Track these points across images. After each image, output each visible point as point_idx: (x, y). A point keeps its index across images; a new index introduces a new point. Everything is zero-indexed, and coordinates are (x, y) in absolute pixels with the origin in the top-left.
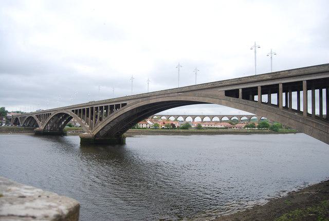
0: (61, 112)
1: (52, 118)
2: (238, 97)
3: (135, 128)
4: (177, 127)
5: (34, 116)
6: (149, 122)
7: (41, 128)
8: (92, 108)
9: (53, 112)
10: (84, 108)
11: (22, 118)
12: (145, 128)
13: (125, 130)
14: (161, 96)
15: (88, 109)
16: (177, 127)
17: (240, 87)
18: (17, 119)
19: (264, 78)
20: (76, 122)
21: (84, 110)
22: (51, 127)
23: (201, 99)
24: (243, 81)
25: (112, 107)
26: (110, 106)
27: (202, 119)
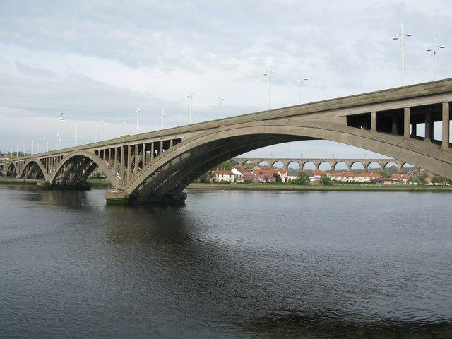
0: (77, 154)
1: (66, 163)
2: (369, 127)
3: (209, 182)
4: (283, 180)
5: (37, 161)
6: (234, 171)
7: (49, 178)
8: (126, 147)
9: (67, 154)
13: (185, 183)
15: (119, 149)
17: (373, 110)
18: (12, 165)
19: (415, 93)
20: (103, 166)
21: (107, 150)
22: (65, 179)
23: (305, 132)
24: (379, 99)
25: (157, 145)
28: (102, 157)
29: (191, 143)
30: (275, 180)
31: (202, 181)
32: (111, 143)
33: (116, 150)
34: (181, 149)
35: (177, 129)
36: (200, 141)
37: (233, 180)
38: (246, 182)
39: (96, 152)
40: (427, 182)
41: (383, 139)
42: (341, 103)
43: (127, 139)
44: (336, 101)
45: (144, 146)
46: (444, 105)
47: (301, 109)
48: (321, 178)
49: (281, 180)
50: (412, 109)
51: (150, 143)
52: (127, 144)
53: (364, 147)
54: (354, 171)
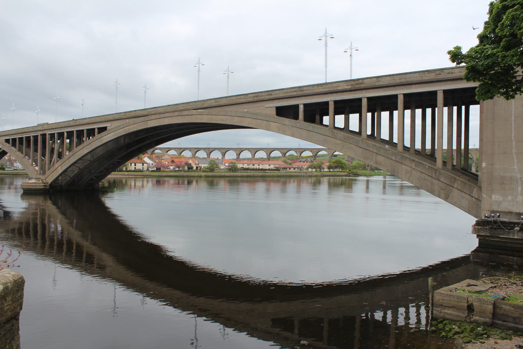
2: (296, 117)
4: (195, 168)
12: (140, 171)
14: (167, 115)
15: (36, 138)
16: (195, 168)
17: (301, 102)
24: (306, 92)
25: (80, 133)
27: (239, 155)
30: (186, 168)
32: (26, 131)
33: (32, 139)
34: (107, 137)
35: (103, 118)
36: (129, 129)
37: (145, 169)
38: (158, 170)
40: (323, 169)
41: (311, 129)
42: (271, 95)
43: (46, 127)
44: (267, 93)
46: (363, 99)
47: (232, 100)
48: (229, 166)
49: (192, 168)
50: (336, 102)
51: (16, 139)
53: (292, 136)
54: (257, 159)
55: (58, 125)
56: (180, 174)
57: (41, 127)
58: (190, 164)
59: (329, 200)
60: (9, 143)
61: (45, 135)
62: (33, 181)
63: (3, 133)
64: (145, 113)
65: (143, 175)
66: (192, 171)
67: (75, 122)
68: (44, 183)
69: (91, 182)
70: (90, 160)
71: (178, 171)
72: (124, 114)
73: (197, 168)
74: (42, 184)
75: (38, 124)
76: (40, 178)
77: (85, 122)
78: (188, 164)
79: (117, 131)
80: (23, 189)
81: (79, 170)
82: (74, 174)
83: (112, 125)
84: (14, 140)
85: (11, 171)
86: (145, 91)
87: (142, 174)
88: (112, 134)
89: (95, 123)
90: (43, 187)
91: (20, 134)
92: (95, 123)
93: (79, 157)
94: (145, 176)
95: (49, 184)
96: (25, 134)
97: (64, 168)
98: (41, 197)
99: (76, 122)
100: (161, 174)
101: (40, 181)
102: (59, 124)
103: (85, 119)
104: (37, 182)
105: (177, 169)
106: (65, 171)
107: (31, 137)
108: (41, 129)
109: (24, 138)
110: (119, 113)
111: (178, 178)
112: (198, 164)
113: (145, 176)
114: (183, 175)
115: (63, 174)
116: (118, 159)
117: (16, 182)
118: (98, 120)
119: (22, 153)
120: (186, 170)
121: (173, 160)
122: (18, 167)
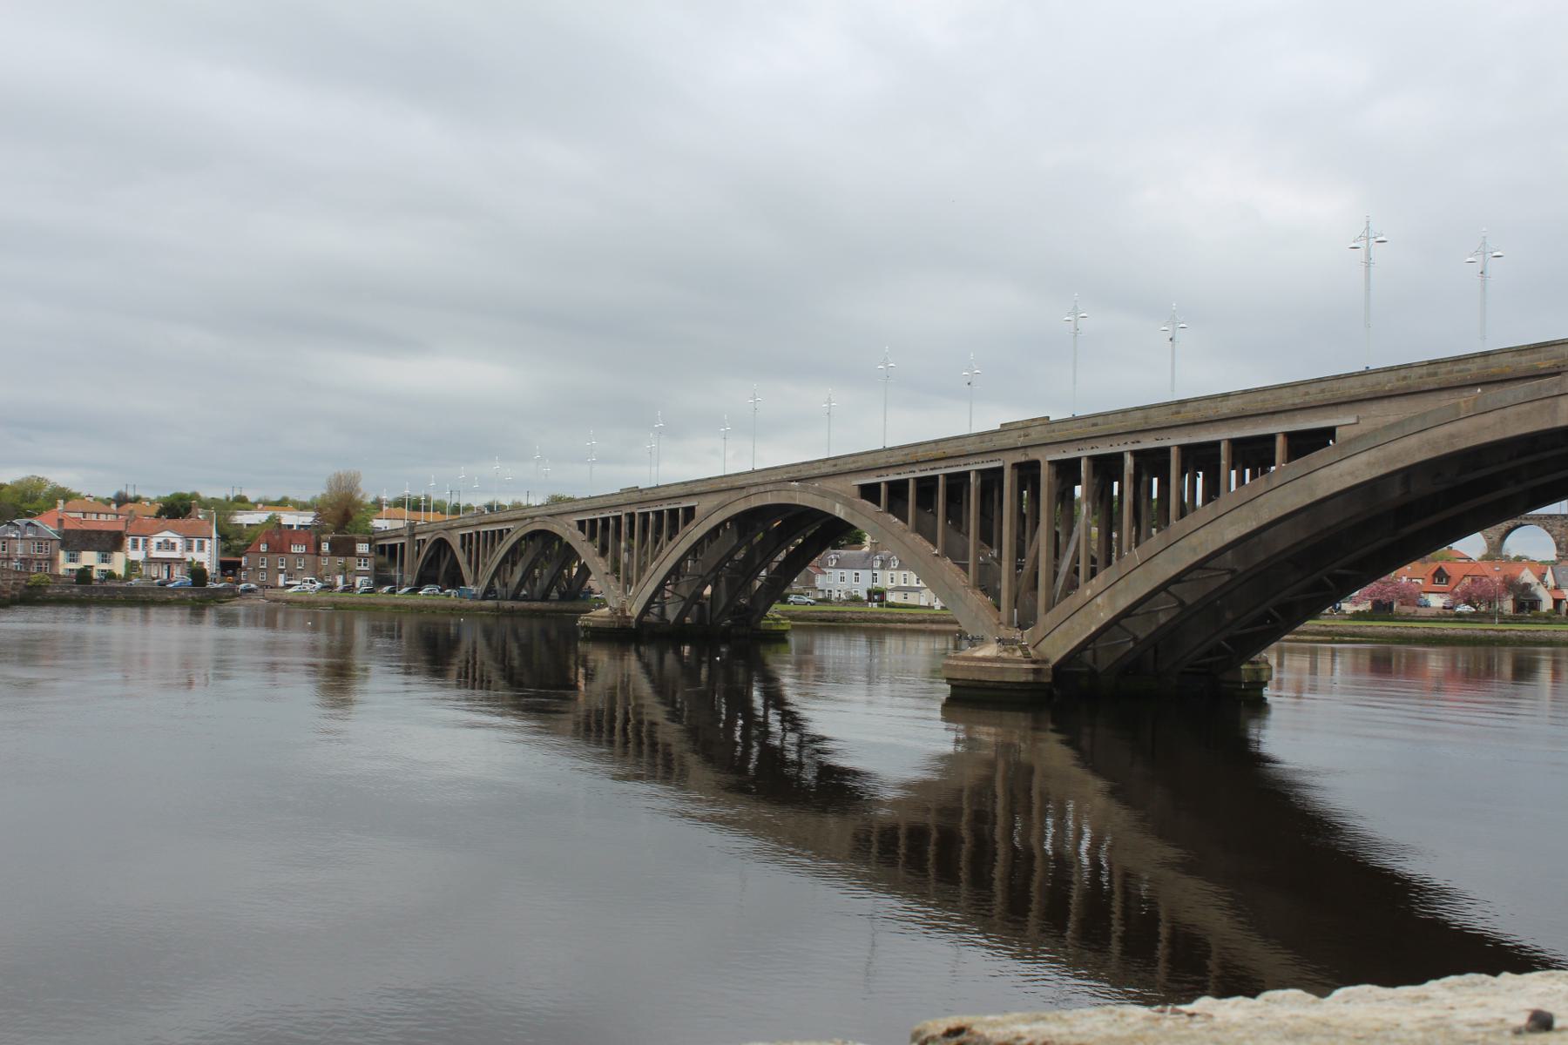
0: (770, 499)
1: (514, 551)
4: (1547, 605)
5: (567, 530)
9: (713, 501)
10: (1071, 454)
11: (478, 543)
16: (1547, 605)
18: (441, 545)
21: (605, 521)
25: (1201, 458)
26: (919, 480)
28: (592, 537)
29: (1395, 448)
30: (1508, 606)
31: (105, 571)
35: (1313, 389)
36: (1452, 436)
39: (581, 524)
43: (1036, 435)
45: (1129, 462)
49: (1535, 603)
52: (1033, 455)
55: (1095, 425)
56: (1490, 633)
57: (1015, 434)
58: (1527, 586)
59: (407, 691)
60: (877, 502)
61: (1035, 464)
62: (990, 650)
63: (854, 462)
64: (1543, 362)
65: (1329, 633)
66: (1536, 617)
67: (1178, 413)
68: (1034, 662)
69: (1208, 660)
70: (1232, 571)
71: (1472, 615)
72: (1424, 370)
73: (1557, 602)
74: (1026, 662)
75: (1002, 425)
76: (1017, 641)
77: (1226, 408)
78: (1518, 586)
79: (1391, 444)
80: (949, 680)
81: (1178, 610)
82: (1154, 628)
83: (1361, 422)
84: (897, 489)
85: (809, 608)
86: (1484, 265)
87: (1323, 628)
88: (1363, 457)
89: (1273, 413)
90: (1031, 678)
91: (923, 467)
92: (1273, 413)
93: (1197, 558)
94: (1337, 638)
95: (1050, 666)
96: (943, 463)
97: (1123, 603)
98: (1021, 714)
99: (1183, 410)
100: (1405, 631)
101: (1014, 650)
102: (1100, 420)
103: (1226, 396)
104: (1005, 655)
105: (1464, 608)
106: (1128, 613)
107: (972, 475)
108: (1019, 445)
109: (941, 481)
110: (1400, 367)
111: (1448, 650)
112: (1557, 588)
113: (1337, 638)
114: (1501, 634)
115: (1116, 627)
116: (1343, 568)
117: (822, 647)
118: (1290, 402)
119: (584, 533)
120: (1506, 613)
121: (1440, 569)
122: (830, 591)
